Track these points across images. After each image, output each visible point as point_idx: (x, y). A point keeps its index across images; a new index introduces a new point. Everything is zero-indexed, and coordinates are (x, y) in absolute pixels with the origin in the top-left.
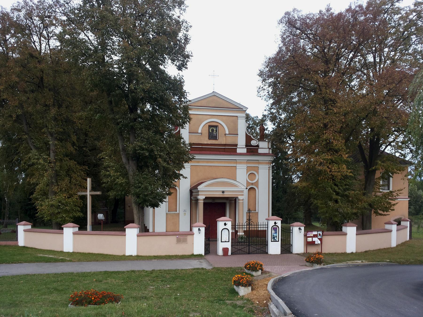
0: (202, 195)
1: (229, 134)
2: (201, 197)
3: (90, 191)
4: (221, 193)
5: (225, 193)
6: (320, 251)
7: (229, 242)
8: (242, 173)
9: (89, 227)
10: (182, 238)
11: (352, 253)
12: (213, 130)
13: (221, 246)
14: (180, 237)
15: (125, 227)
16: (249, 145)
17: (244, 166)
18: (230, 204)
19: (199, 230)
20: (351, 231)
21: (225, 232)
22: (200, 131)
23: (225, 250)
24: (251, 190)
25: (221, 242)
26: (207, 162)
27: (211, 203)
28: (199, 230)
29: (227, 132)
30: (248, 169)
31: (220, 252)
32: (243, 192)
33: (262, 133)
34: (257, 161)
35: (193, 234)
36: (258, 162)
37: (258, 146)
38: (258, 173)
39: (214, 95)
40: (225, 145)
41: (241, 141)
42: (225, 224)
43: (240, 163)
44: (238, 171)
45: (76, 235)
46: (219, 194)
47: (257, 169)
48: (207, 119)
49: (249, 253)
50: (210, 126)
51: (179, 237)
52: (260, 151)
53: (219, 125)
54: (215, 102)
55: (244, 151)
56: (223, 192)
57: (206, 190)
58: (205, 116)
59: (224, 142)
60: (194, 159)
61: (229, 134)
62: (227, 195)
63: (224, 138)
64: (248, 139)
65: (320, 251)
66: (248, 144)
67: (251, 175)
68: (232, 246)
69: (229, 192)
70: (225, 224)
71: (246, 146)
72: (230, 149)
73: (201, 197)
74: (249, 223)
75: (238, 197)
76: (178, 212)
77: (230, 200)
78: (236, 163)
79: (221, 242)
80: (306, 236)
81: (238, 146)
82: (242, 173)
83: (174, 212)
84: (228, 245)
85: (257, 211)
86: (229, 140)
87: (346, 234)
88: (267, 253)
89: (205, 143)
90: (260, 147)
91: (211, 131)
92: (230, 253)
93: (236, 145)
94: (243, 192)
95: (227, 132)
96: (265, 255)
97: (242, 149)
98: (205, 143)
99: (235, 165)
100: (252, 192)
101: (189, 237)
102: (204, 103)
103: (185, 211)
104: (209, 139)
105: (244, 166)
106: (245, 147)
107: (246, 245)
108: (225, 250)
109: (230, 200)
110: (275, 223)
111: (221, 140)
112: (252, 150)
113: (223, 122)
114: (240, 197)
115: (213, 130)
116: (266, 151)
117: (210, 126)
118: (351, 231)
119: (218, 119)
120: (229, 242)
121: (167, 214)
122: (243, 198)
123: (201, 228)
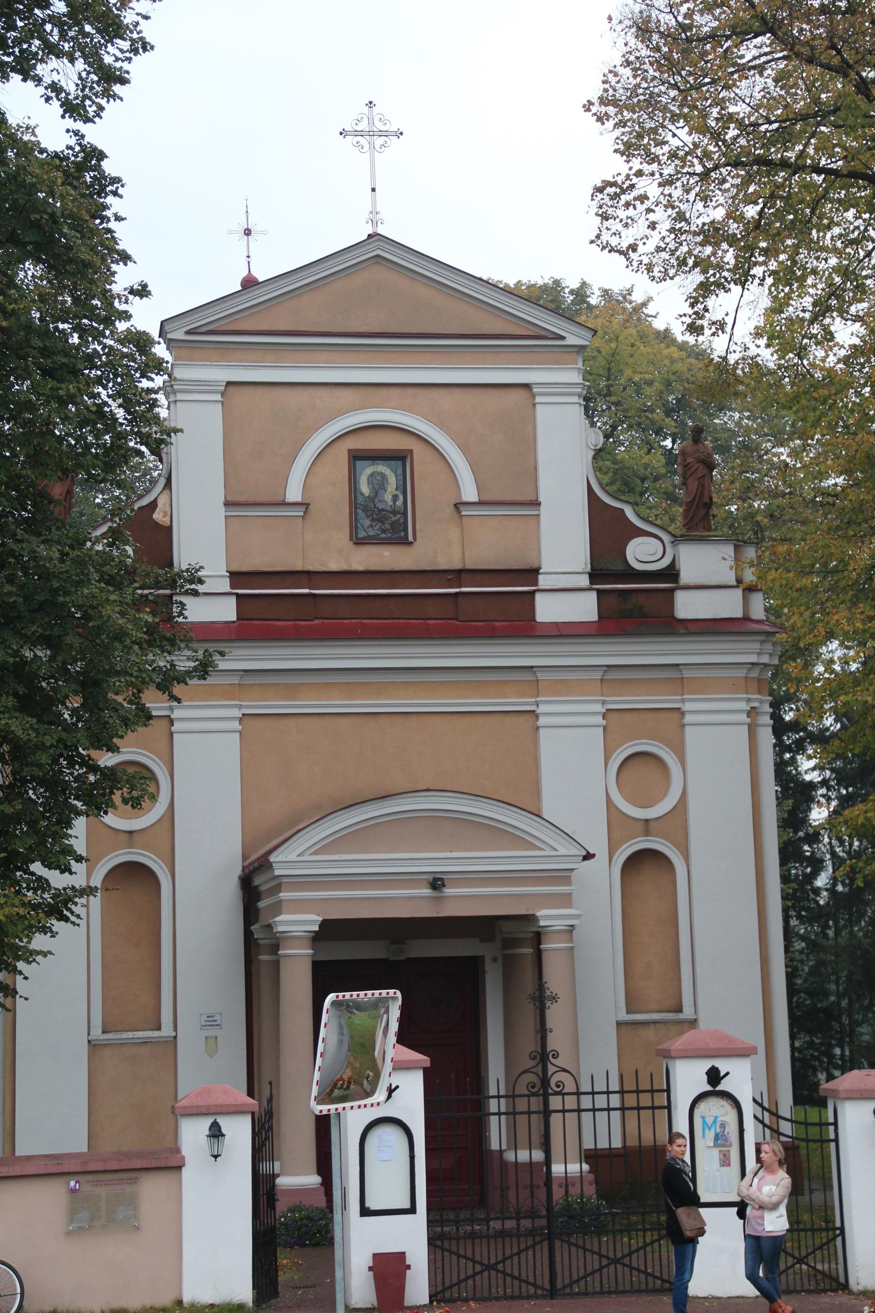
0: (300, 906)
1: (480, 503)
2: (296, 922)
4: (427, 891)
5: (449, 891)
7: (412, 1210)
8: (574, 766)
10: (102, 1191)
12: (378, 483)
13: (361, 1241)
14: (87, 1188)
18: (510, 967)
19: (216, 1133)
22: (294, 494)
23: (389, 1269)
24: (645, 866)
25: (365, 1212)
26: (350, 690)
27: (385, 961)
28: (216, 1133)
29: (470, 493)
30: (615, 724)
31: (358, 1284)
32: (567, 881)
33: (693, 485)
34: (526, 676)
36: (675, 677)
37: (671, 574)
39: (378, 258)
40: (458, 575)
41: (563, 546)
43: (562, 688)
44: (550, 744)
46: (410, 902)
49: (553, 1293)
50: (357, 457)
51: (87, 1186)
52: (687, 606)
53: (419, 452)
54: (379, 296)
55: (584, 608)
56: (437, 883)
57: (353, 870)
61: (480, 503)
62: (462, 901)
63: (454, 533)
64: (608, 532)
66: (606, 567)
67: (640, 769)
68: (434, 1241)
69: (477, 880)
71: (596, 575)
72: (491, 604)
73: (296, 922)
74: (545, 1081)
76: (166, 1030)
77: (510, 943)
79: (365, 1212)
81: (543, 581)
82: (574, 766)
83: (150, 1034)
84: (411, 1237)
85: (688, 1012)
86: (487, 545)
88: (839, 1284)
90: (685, 577)
92: (418, 1287)
93: (531, 574)
94: (567, 881)
95: (470, 493)
96: (841, 1298)
97: (566, 600)
98: (333, 566)
99: (524, 703)
100: (648, 880)
101: (150, 1188)
102: (312, 312)
103: (211, 1022)
104: (359, 542)
106: (584, 581)
107: (532, 1232)
108: (389, 1269)
109: (510, 943)
110: (714, 1076)
111: (437, 545)
112: (633, 604)
113: (442, 426)
114: (549, 917)
115: (378, 483)
116: (727, 605)
117: (357, 457)
119: (408, 409)
120: (412, 1210)
121: (92, 1045)
122: (588, 921)
123: (225, 1123)
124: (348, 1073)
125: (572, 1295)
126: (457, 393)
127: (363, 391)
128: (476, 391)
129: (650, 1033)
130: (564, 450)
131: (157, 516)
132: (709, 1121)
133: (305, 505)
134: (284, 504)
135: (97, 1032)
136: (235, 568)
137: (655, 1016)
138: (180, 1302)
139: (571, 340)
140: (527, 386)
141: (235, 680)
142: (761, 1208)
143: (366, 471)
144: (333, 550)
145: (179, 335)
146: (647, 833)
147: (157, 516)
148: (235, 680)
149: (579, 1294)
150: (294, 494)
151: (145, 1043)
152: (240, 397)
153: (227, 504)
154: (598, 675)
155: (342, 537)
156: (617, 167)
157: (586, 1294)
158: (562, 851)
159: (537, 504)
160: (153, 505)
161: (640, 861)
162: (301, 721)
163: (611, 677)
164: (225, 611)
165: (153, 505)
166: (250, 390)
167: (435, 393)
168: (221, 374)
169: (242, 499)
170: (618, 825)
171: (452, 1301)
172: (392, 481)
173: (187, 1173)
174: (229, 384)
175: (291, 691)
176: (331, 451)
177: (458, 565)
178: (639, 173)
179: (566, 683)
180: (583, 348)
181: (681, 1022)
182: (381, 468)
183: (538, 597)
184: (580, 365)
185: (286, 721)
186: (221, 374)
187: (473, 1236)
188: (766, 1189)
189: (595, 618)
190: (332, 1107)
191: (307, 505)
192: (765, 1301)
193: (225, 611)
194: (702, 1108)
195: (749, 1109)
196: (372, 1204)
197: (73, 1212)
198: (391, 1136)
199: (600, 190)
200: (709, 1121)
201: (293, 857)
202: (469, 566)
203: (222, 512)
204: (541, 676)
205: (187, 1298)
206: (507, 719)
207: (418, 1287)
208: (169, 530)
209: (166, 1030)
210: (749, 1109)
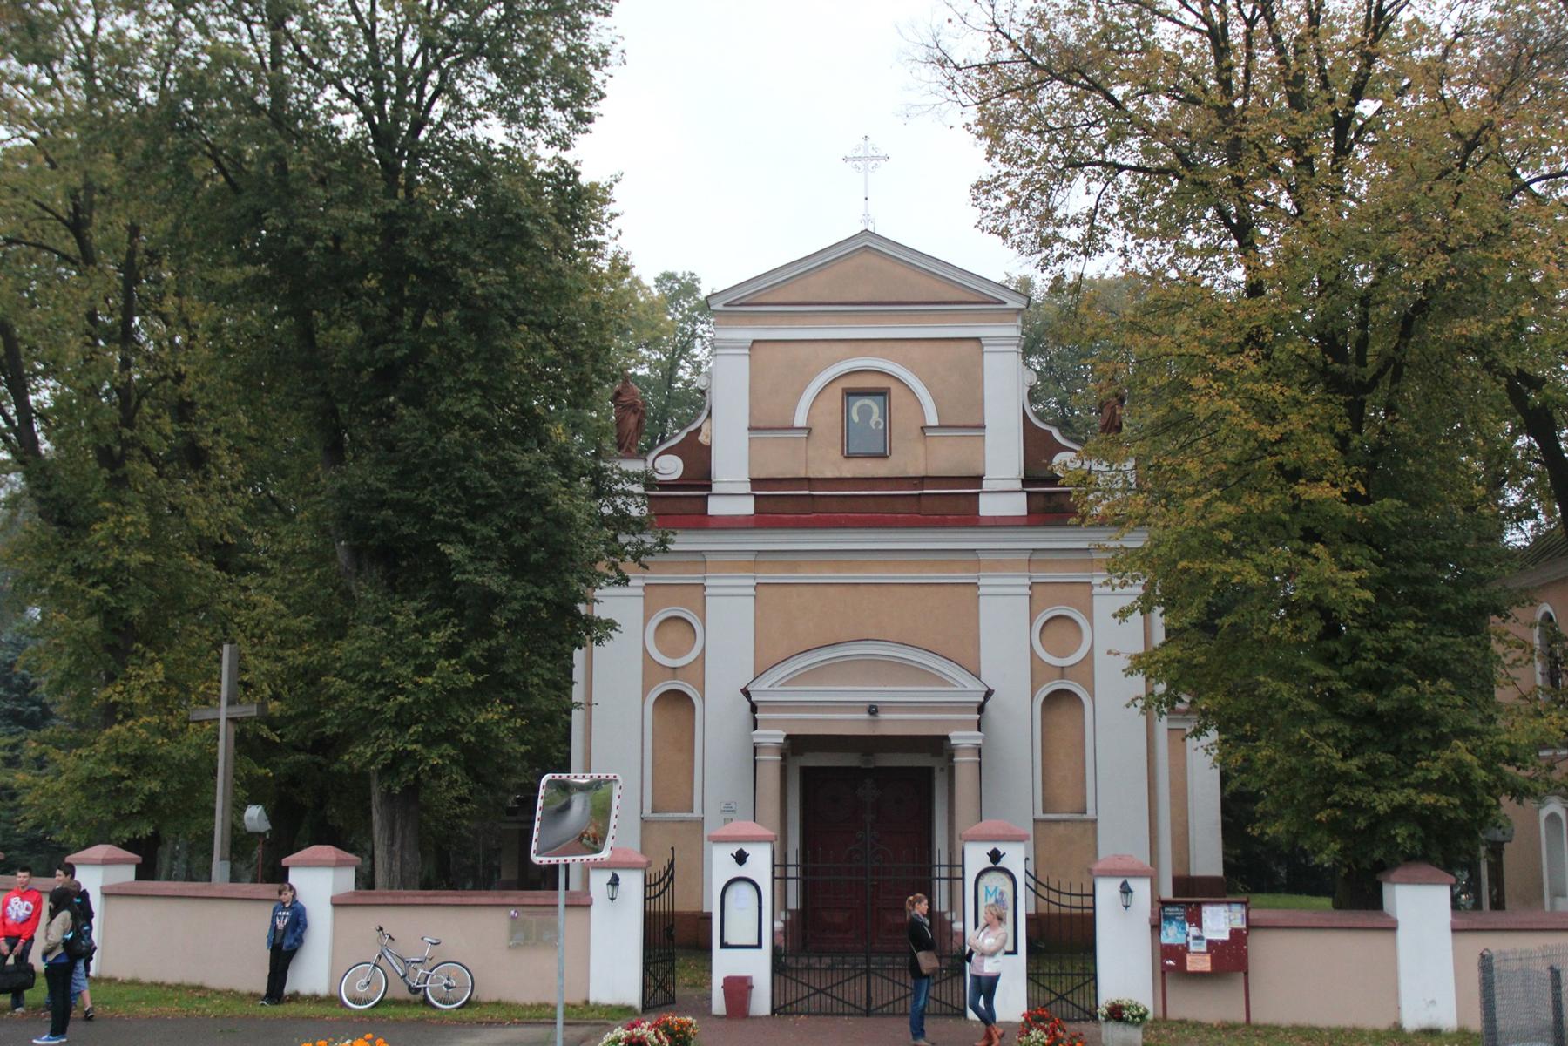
3: (231, 703)
4: (866, 716)
5: (882, 716)
6: (1243, 1018)
7: (759, 946)
9: (220, 868)
10: (534, 919)
11: (1432, 1033)
12: (865, 413)
15: (285, 862)
16: (1046, 474)
17: (1018, 583)
19: (1126, 890)
20: (1421, 907)
21: (742, 898)
22: (800, 420)
23: (738, 989)
24: (1060, 702)
26: (837, 566)
27: (858, 768)
29: (932, 420)
34: (971, 557)
35: (588, 906)
38: (1090, 617)
40: (922, 481)
41: (1002, 459)
42: (741, 858)
44: (714, 606)
45: (113, 901)
46: (853, 724)
47: (1083, 595)
48: (845, 358)
53: (895, 390)
54: (867, 277)
55: (1017, 505)
56: (873, 710)
58: (825, 345)
59: (915, 469)
60: (665, 551)
61: (940, 427)
62: (892, 724)
64: (1037, 446)
65: (1240, 1017)
66: (1036, 477)
67: (1058, 628)
68: (778, 967)
69: (906, 706)
70: (741, 858)
72: (947, 502)
73: (771, 736)
75: (946, 738)
76: (697, 813)
78: (977, 565)
79: (724, 945)
80: (1156, 928)
81: (986, 485)
84: (757, 967)
85: (1090, 814)
86: (943, 458)
87: (1392, 928)
89: (829, 473)
91: (855, 417)
92: (761, 1002)
93: (977, 480)
95: (932, 420)
97: (1003, 500)
98: (829, 475)
99: (968, 577)
102: (816, 288)
105: (1018, 583)
106: (1018, 485)
110: (995, 856)
111: (908, 460)
112: (1049, 502)
113: (912, 369)
114: (963, 738)
117: (850, 393)
118: (1421, 907)
119: (888, 358)
120: (759, 946)
123: (1132, 883)
124: (592, 830)
125: (882, 1014)
126: (925, 345)
127: (853, 344)
128: (937, 344)
129: (1061, 829)
130: (1006, 384)
131: (701, 438)
132: (991, 890)
133: (809, 430)
134: (792, 428)
135: (648, 812)
136: (755, 476)
137: (1065, 816)
138: (587, 1002)
139: (1011, 304)
140: (978, 339)
141: (751, 558)
142: (983, 954)
143: (858, 403)
144: (828, 463)
145: (719, 307)
146: (1062, 677)
147: (701, 438)
148: (751, 558)
149: (888, 1014)
150: (800, 420)
151: (682, 821)
152: (763, 351)
153: (751, 429)
154: (1026, 556)
155: (835, 453)
156: (987, 171)
157: (893, 1014)
158: (970, 688)
159: (983, 427)
160: (699, 430)
161: (1058, 699)
162: (801, 588)
163: (1035, 558)
164: (747, 507)
165: (699, 430)
166: (768, 346)
167: (909, 345)
168: (748, 334)
169: (761, 425)
170: (1038, 670)
171: (791, 1014)
172: (876, 409)
173: (594, 910)
174: (755, 341)
175: (793, 567)
176: (829, 389)
177: (923, 474)
178: (1007, 174)
179: (1000, 563)
180: (1020, 310)
181: (1085, 821)
182: (867, 401)
183: (981, 497)
184: (1019, 323)
185: (789, 588)
186: (748, 334)
187: (809, 968)
188: (987, 941)
189: (1025, 513)
190: (561, 860)
191: (809, 430)
192: (983, 1026)
193: (747, 507)
194: (987, 880)
195: (1021, 879)
196: (729, 939)
197: (513, 932)
198: (745, 891)
199: (976, 187)
200: (991, 890)
201: (765, 687)
202: (931, 474)
203: (746, 434)
204: (982, 557)
205: (592, 1000)
206: (956, 589)
207: (761, 1002)
208: (709, 448)
209: (697, 813)
210: (1021, 879)
